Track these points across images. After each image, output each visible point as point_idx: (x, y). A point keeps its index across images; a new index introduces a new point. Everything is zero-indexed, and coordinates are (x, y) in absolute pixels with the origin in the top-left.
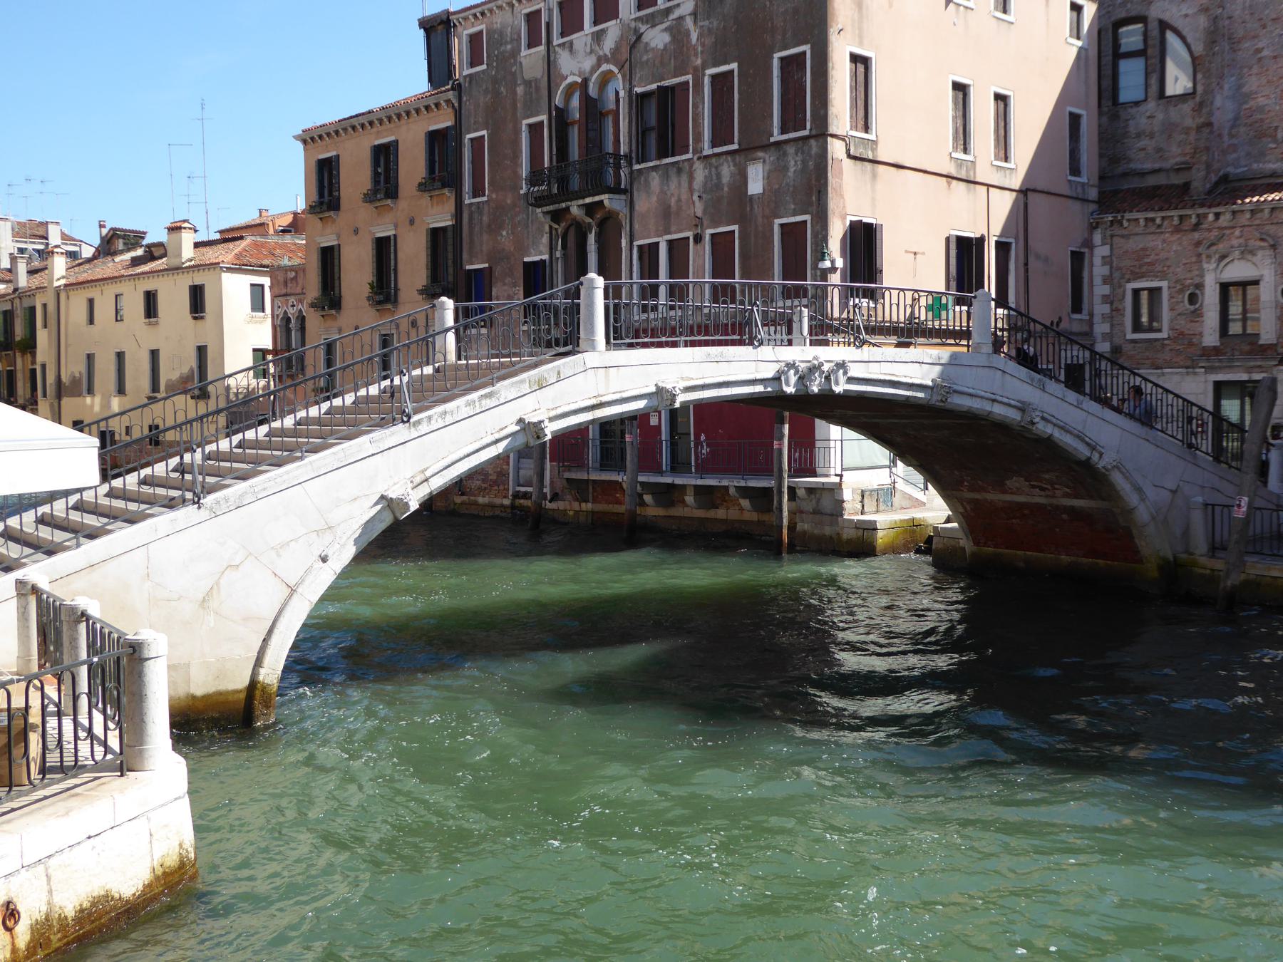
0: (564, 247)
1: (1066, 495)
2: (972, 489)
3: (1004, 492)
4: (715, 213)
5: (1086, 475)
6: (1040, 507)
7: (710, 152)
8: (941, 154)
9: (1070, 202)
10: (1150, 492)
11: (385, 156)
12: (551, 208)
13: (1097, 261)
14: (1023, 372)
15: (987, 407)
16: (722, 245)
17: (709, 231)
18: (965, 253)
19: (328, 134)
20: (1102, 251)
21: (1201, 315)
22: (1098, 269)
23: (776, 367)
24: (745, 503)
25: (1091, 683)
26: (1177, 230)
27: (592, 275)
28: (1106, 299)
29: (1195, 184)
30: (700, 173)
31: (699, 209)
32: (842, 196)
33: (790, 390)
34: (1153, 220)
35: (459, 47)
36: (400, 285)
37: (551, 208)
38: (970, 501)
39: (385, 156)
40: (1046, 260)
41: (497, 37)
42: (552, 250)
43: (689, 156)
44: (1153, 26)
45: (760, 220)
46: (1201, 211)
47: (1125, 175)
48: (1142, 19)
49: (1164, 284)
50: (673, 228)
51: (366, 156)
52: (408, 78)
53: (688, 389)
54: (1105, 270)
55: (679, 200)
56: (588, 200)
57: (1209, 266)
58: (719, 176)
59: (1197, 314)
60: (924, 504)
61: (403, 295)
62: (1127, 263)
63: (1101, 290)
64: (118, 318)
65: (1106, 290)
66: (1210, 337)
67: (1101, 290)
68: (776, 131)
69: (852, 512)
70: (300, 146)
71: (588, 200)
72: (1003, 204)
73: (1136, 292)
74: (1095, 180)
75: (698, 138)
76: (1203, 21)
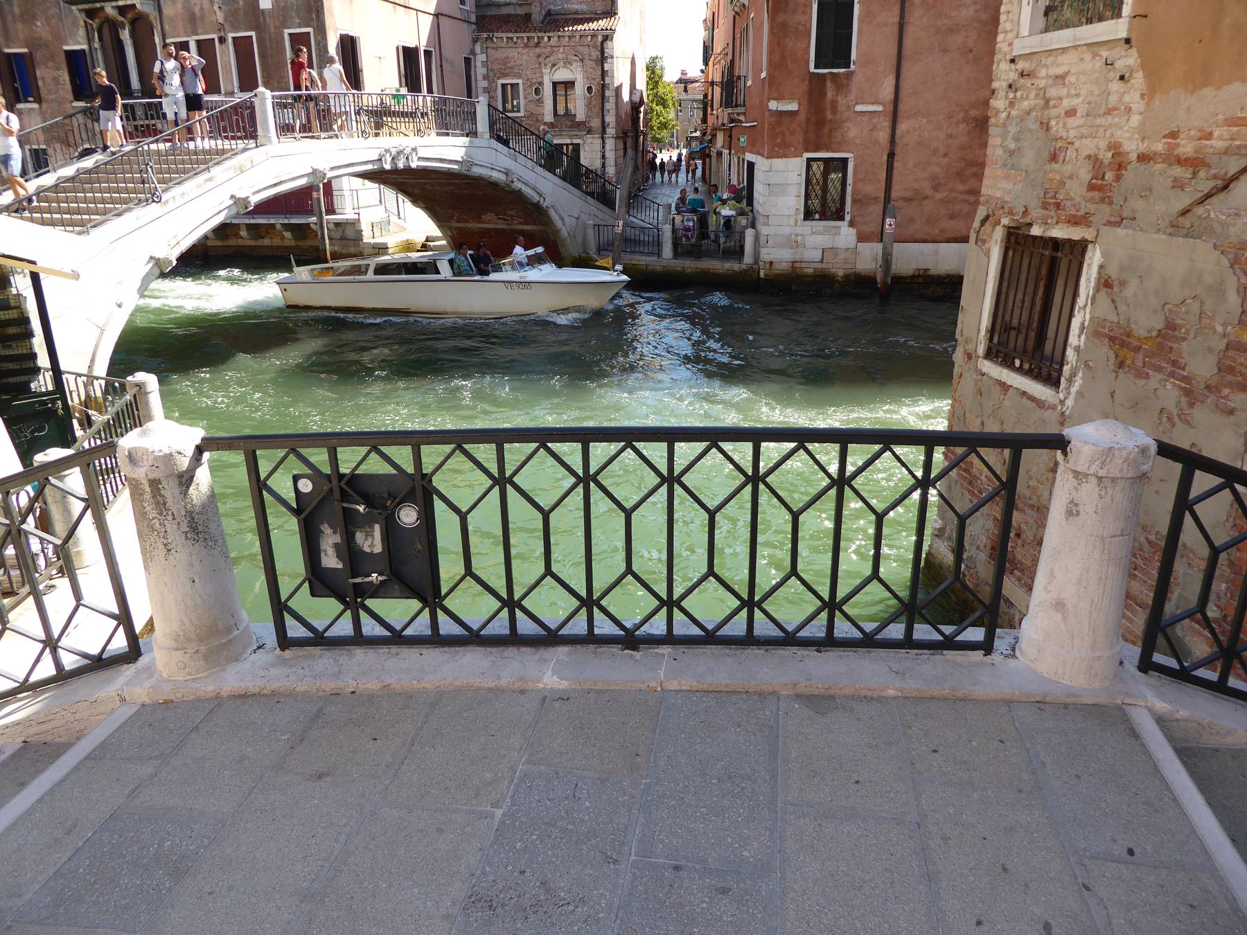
0: (101, 39)
1: (521, 223)
2: (458, 221)
3: (480, 222)
4: (234, 20)
6: (502, 230)
10: (566, 218)
12: (86, 6)
13: (479, 64)
14: (500, 146)
16: (242, 46)
17: (230, 35)
18: (409, 56)
20: (481, 58)
22: (480, 71)
23: (378, 152)
24: (288, 235)
25: (378, 320)
26: (526, 46)
27: (261, 89)
29: (534, 16)
31: (220, 17)
33: (387, 167)
37: (86, 6)
38: (456, 228)
40: (451, 63)
42: (90, 41)
45: (272, 29)
46: (540, 34)
49: (520, 81)
53: (332, 169)
54: (484, 71)
55: (202, 9)
57: (546, 71)
59: (540, 101)
62: (496, 66)
63: (483, 84)
65: (485, 84)
66: (549, 118)
67: (483, 84)
69: (367, 238)
72: (426, 22)
73: (504, 86)
74: (474, 9)
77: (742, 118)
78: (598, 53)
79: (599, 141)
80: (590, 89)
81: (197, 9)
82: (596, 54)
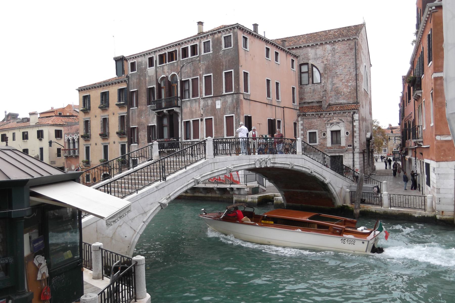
5: (324, 186)
7: (205, 97)
8: (265, 99)
9: (293, 110)
11: (105, 96)
13: (300, 125)
15: (301, 169)
16: (209, 121)
19: (87, 89)
21: (326, 139)
22: (300, 127)
26: (320, 117)
28: (302, 135)
30: (202, 102)
32: (243, 109)
33: (257, 167)
34: (313, 115)
35: (128, 66)
36: (110, 132)
39: (105, 96)
41: (140, 64)
43: (199, 97)
44: (310, 66)
47: (305, 103)
48: (307, 64)
50: (194, 117)
51: (99, 95)
52: (110, 73)
54: (302, 127)
55: (196, 109)
56: (169, 109)
58: (207, 103)
59: (325, 139)
60: (265, 191)
61: (111, 134)
62: (307, 125)
63: (301, 132)
64: (14, 139)
65: (302, 132)
68: (224, 92)
70: (78, 92)
71: (169, 109)
75: (201, 93)
76: (322, 64)
77: (421, 144)
78: (351, 119)
79: (351, 155)
80: (347, 133)
81: (194, 110)
82: (350, 119)
